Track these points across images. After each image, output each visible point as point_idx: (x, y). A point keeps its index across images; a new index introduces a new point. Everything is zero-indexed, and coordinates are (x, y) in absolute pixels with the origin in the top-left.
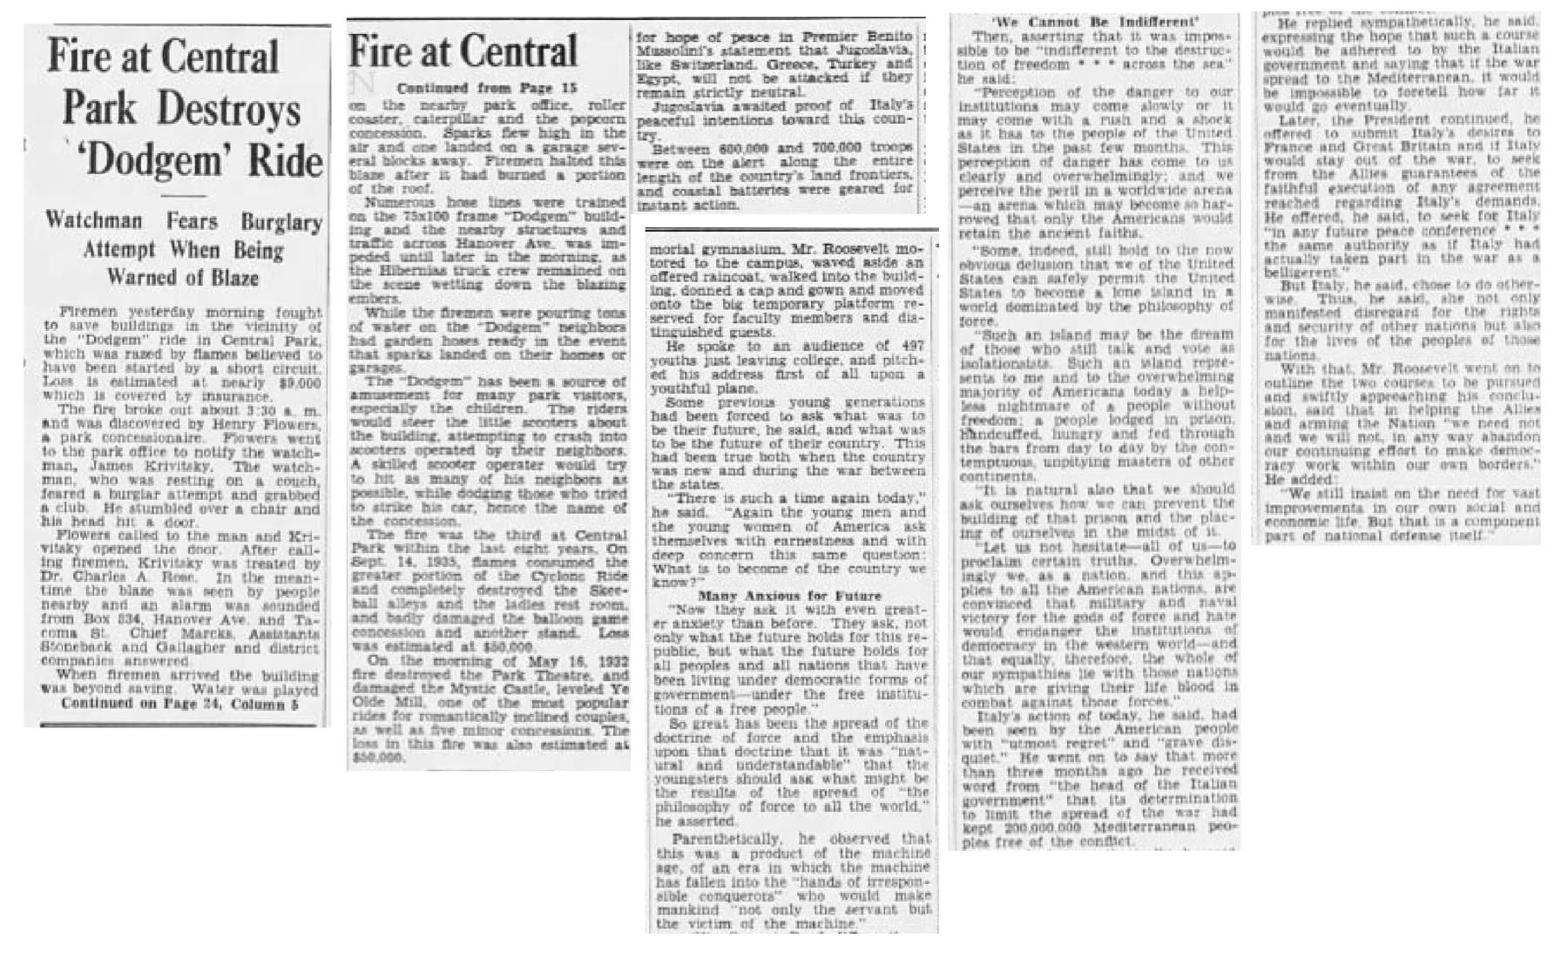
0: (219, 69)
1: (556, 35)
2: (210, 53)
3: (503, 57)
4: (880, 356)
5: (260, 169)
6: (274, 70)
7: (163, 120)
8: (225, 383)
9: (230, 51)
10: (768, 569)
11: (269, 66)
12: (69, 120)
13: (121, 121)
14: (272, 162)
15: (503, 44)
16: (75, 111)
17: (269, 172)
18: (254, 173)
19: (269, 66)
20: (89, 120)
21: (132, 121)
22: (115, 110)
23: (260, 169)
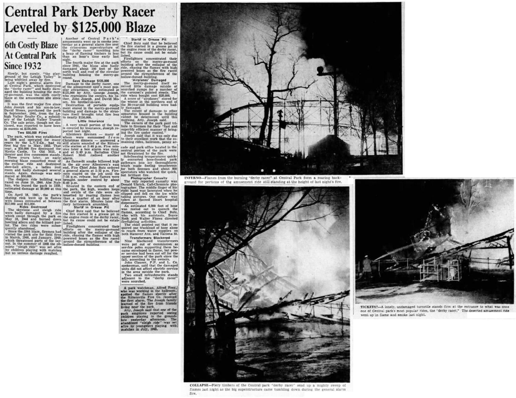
0: (26, 16)
1: (5, 23)
2: (22, 11)
3: (21, 13)
4: (83, 41)
5: (127, 14)
6: (45, 16)
7: (85, 15)
8: (83, 105)
9: (29, 10)
10: (34, 98)
11: (44, 14)
12: (54, 15)
13: (73, 16)
14: (130, 12)
15: (98, 10)
16: (56, 13)
17: (129, 15)
18: (125, 15)
19: (44, 14)
20: (61, 15)
21: (76, 16)
22: (52, 56)
23: (127, 14)
